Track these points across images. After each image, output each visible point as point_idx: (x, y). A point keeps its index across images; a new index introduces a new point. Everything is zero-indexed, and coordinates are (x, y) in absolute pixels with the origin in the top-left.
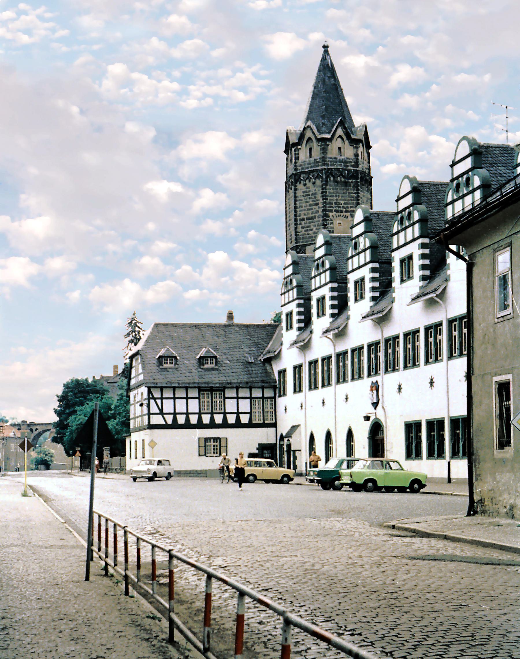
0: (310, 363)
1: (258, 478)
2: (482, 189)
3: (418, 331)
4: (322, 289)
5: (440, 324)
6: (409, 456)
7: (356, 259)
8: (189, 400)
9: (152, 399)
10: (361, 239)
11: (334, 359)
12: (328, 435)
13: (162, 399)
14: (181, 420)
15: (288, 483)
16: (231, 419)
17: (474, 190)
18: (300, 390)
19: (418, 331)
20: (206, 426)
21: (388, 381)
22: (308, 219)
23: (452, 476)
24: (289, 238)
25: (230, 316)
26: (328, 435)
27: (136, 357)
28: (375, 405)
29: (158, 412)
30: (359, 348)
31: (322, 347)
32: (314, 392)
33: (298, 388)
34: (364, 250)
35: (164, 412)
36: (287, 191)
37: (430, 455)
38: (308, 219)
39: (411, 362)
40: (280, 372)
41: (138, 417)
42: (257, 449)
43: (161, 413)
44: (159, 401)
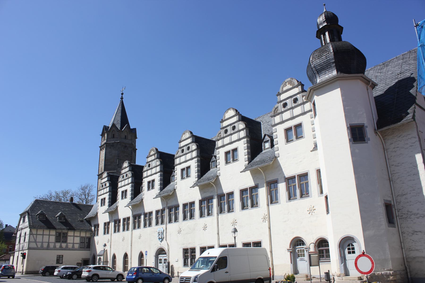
1: (100, 277)
4: (125, 184)
10: (153, 162)
12: (126, 256)
13: (37, 234)
14: (45, 245)
15: (121, 281)
16: (70, 246)
17: (192, 151)
20: (70, 250)
21: (172, 227)
25: (72, 199)
26: (126, 256)
28: (162, 239)
34: (156, 166)
35: (37, 241)
39: (126, 228)
41: (36, 244)
43: (36, 242)
44: (35, 236)
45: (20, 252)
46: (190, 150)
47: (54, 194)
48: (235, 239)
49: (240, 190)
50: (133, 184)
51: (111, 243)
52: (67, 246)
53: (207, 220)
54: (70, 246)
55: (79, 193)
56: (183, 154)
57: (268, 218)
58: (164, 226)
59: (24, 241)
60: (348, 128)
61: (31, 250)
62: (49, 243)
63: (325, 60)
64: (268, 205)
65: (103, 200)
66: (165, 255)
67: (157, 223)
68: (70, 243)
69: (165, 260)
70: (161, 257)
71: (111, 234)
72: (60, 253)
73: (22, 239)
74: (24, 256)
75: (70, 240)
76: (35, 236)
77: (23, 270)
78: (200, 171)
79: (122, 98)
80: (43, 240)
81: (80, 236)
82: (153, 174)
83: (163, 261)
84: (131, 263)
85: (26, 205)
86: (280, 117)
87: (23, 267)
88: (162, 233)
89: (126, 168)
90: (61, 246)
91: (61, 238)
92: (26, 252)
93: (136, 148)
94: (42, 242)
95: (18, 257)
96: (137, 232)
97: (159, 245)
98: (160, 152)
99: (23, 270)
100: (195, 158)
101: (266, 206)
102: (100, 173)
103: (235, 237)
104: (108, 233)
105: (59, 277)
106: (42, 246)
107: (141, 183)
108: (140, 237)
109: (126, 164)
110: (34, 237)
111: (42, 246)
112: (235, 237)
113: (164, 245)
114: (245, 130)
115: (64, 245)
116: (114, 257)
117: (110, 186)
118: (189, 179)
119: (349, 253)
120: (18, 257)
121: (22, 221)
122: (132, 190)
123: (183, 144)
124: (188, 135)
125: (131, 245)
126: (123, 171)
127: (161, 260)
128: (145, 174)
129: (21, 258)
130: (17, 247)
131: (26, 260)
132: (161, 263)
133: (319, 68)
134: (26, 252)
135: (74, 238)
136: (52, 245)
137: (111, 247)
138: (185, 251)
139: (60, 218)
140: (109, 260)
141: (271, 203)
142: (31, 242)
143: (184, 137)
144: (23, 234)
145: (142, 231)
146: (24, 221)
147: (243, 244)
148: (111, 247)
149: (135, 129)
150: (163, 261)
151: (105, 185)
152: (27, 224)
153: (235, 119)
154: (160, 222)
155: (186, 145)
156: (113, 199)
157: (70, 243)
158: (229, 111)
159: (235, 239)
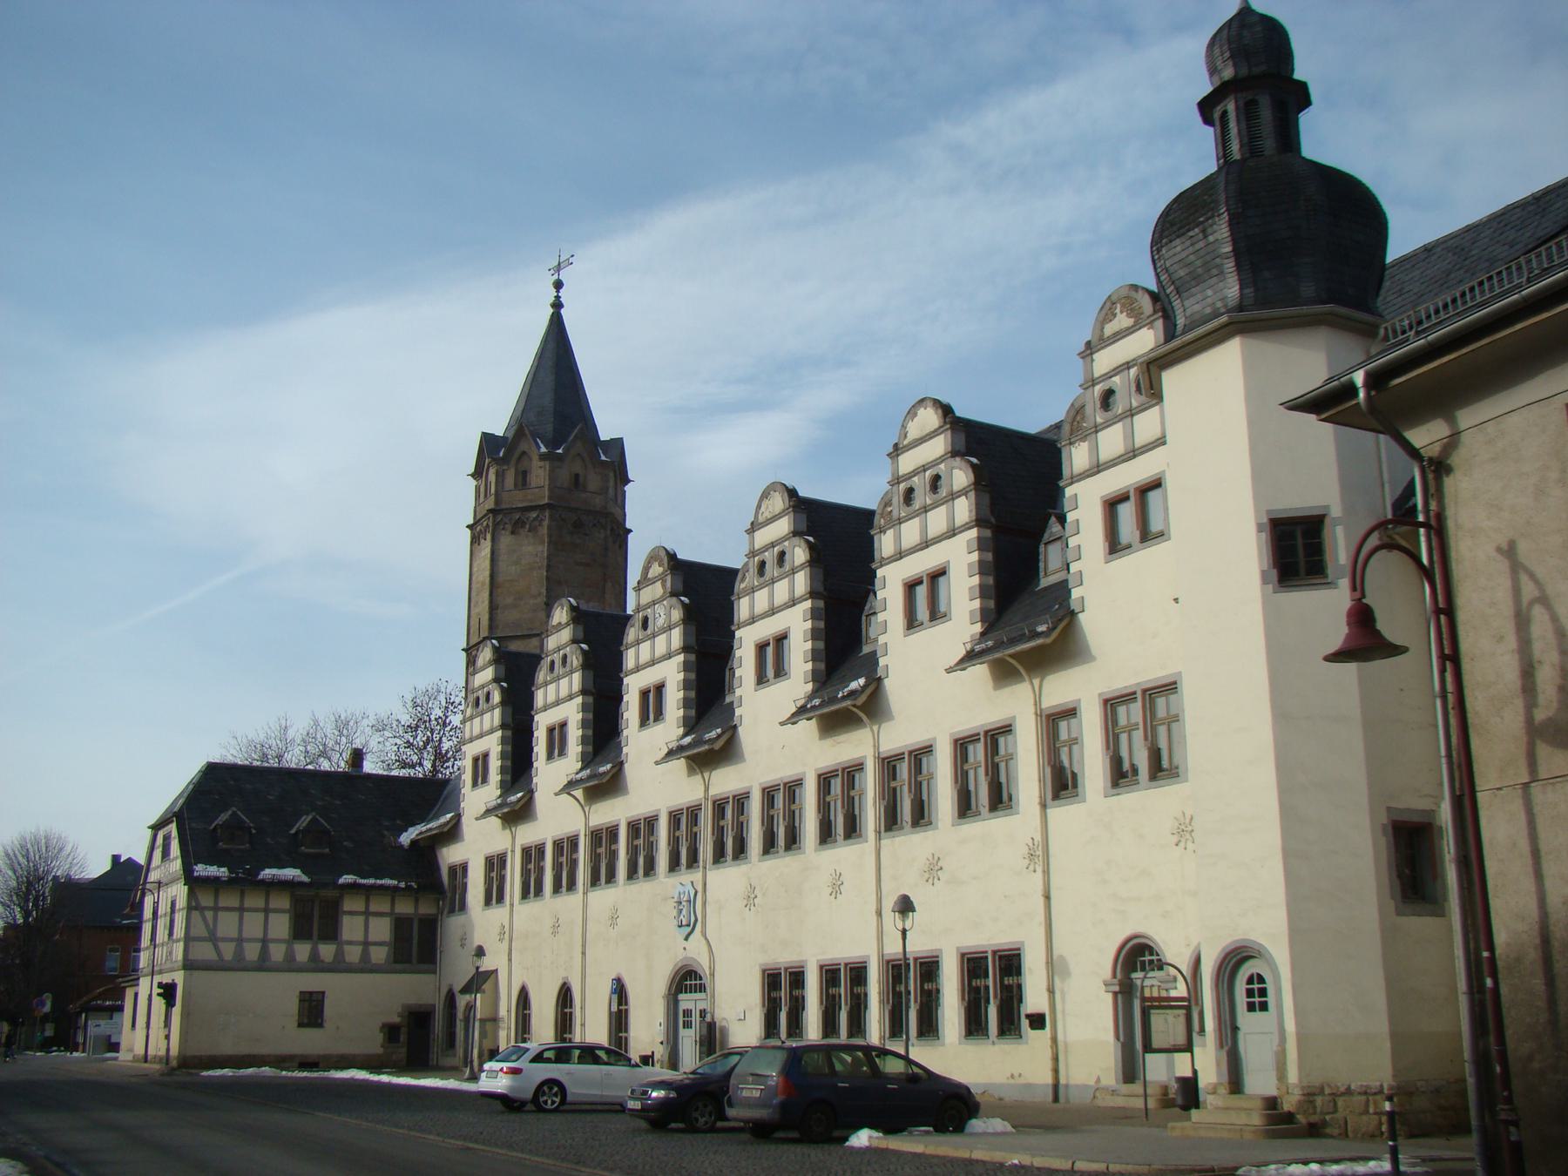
0: (526, 852)
3: (928, 750)
4: (560, 702)
5: (859, 767)
8: (272, 916)
9: (196, 908)
11: (755, 807)
12: (565, 996)
13: (216, 909)
14: (252, 952)
16: (353, 954)
17: (953, 496)
19: (928, 750)
20: (301, 969)
24: (474, 622)
26: (565, 996)
29: (206, 934)
30: (1144, 691)
31: (558, 813)
33: (495, 894)
34: (670, 628)
35: (220, 934)
36: (475, 540)
39: (565, 882)
40: (453, 870)
42: (399, 1015)
43: (213, 938)
45: (157, 979)
46: (943, 492)
47: (298, 729)
48: (904, 938)
49: (956, 741)
50: (509, 733)
51: (511, 941)
52: (339, 954)
53: (844, 855)
54: (353, 954)
55: (406, 719)
56: (1109, 414)
57: (1041, 854)
58: (697, 876)
59: (171, 934)
60: (1260, 528)
61: (196, 973)
62: (265, 941)
63: (1201, 244)
64: (1044, 806)
65: (481, 762)
66: (702, 995)
67: (674, 865)
68: (350, 943)
69: (703, 1013)
70: (687, 1001)
71: (512, 905)
73: (162, 924)
74: (168, 992)
75: (351, 928)
76: (209, 915)
77: (168, 1050)
78: (993, 592)
79: (557, 305)
80: (240, 931)
81: (391, 914)
82: (656, 661)
83: (696, 1019)
84: (583, 1025)
85: (172, 781)
86: (1090, 450)
87: (167, 1037)
88: (691, 902)
89: (559, 627)
90: (314, 956)
91: (316, 918)
92: (178, 977)
93: (628, 526)
94: (240, 940)
95: (150, 996)
96: (603, 898)
97: (681, 955)
98: (960, 420)
99: (168, 1050)
100: (966, 527)
101: (1038, 808)
102: (473, 642)
103: (904, 932)
104: (500, 899)
106: (239, 952)
107: (618, 698)
108: (614, 919)
109: (560, 615)
110: (204, 919)
111: (239, 952)
112: (904, 932)
113: (696, 950)
114: (972, 495)
115: (327, 951)
116: (524, 999)
117: (503, 703)
119: (1251, 1007)
120: (150, 996)
121: (158, 854)
122: (686, 685)
123: (907, 462)
124: (929, 418)
125: (584, 953)
126: (552, 642)
127: (687, 1013)
128: (743, 608)
129: (159, 1004)
130: (144, 959)
131: (177, 1011)
132: (687, 1025)
133: (1182, 273)
134: (178, 977)
135: (366, 927)
136: (277, 953)
137: (510, 960)
138: (772, 980)
139: (309, 837)
140: (503, 1012)
141: (1056, 797)
143: (914, 430)
144: (164, 908)
145: (622, 896)
146: (166, 853)
147: (963, 955)
148: (510, 960)
149: (617, 445)
150: (696, 1019)
151: (488, 699)
153: (939, 446)
154: (684, 860)
155: (773, 545)
156: (519, 766)
157: (350, 943)
158: (921, 412)
159: (904, 938)
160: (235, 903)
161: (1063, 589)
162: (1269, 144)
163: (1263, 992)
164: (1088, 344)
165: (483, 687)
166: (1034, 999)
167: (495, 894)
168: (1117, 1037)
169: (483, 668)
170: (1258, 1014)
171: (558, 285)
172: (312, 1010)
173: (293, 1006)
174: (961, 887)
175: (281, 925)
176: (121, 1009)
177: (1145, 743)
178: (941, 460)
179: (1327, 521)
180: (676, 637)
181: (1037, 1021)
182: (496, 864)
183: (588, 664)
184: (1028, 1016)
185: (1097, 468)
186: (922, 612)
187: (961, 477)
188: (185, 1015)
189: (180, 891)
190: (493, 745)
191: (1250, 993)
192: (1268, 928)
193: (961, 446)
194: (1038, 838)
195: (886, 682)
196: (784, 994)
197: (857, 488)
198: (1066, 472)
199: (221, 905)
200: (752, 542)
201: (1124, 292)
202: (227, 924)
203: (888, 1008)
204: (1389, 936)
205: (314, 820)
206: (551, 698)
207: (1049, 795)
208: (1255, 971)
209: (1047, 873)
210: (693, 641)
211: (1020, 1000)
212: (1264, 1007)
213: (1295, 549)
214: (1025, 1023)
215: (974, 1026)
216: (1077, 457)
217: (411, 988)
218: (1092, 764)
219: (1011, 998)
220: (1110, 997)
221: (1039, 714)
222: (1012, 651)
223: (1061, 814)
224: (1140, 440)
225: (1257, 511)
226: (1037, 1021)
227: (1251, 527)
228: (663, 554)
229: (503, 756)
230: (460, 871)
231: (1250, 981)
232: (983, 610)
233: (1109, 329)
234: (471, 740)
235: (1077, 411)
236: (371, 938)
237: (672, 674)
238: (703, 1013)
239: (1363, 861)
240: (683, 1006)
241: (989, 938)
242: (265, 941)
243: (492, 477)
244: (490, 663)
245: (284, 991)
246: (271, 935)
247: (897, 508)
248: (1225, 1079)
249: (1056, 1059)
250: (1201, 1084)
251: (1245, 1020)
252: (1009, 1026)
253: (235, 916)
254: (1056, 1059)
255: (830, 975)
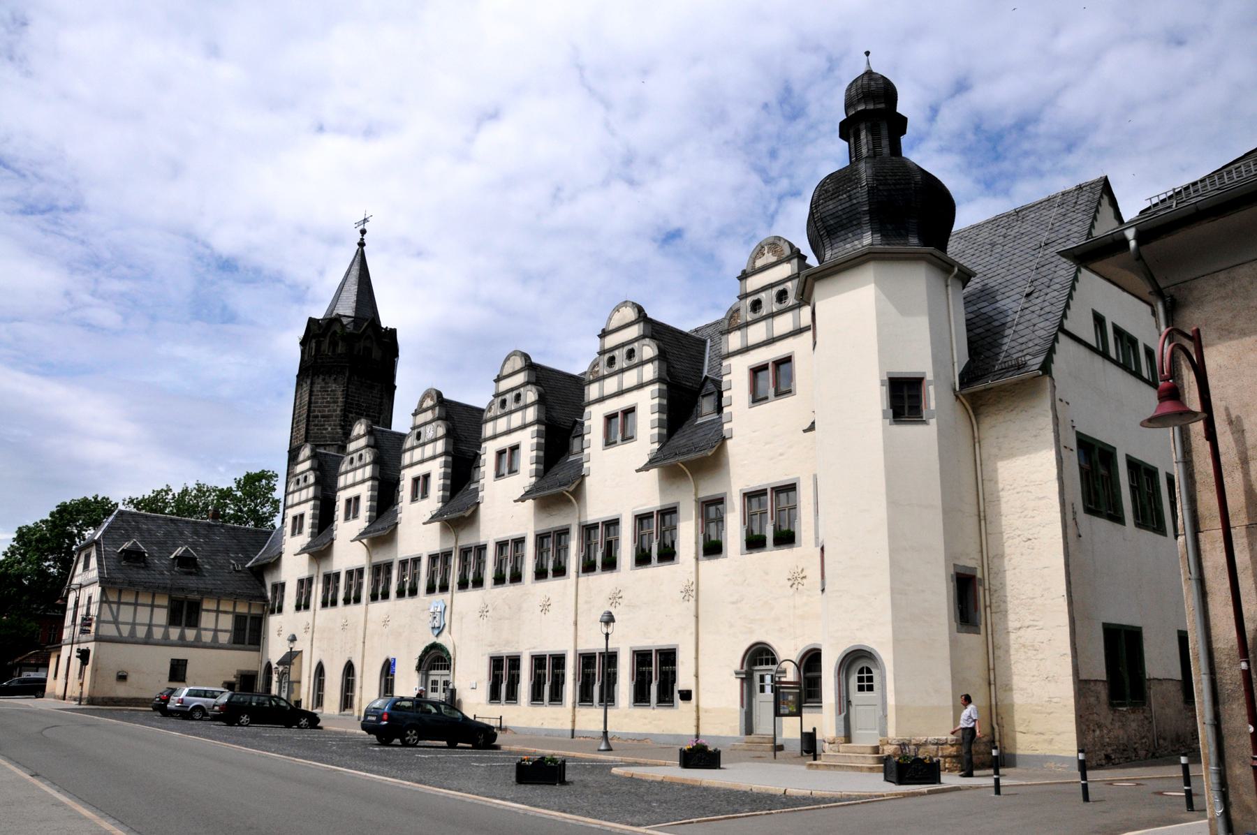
2: (656, 363)
4: (356, 483)
6: (494, 696)
7: (297, 494)
12: (349, 669)
13: (119, 603)
14: (141, 632)
16: (207, 637)
17: (526, 407)
18: (307, 607)
20: (205, 646)
22: (323, 417)
23: (577, 728)
26: (349, 669)
27: (87, 551)
32: (330, 611)
33: (303, 604)
34: (435, 440)
35: (121, 619)
36: (299, 385)
37: (537, 696)
38: (323, 417)
39: (353, 598)
43: (116, 622)
45: (75, 647)
50: (376, 483)
52: (198, 637)
54: (207, 637)
57: (693, 592)
58: (446, 596)
62: (150, 626)
64: (697, 559)
65: (298, 520)
72: (180, 653)
74: (84, 655)
75: (207, 620)
76: (114, 607)
79: (362, 244)
82: (426, 461)
87: (82, 684)
88: (443, 613)
90: (182, 637)
91: (184, 613)
103: (607, 635)
104: (307, 607)
105: (74, 704)
106: (133, 632)
107: (397, 482)
108: (386, 623)
110: (111, 609)
111: (133, 632)
112: (607, 635)
115: (190, 634)
116: (320, 670)
118: (425, 502)
119: (861, 689)
126: (352, 446)
127: (435, 683)
128: (407, 458)
129: (76, 663)
131: (88, 668)
134: (91, 646)
135: (217, 621)
136: (158, 633)
138: (496, 662)
142: (104, 622)
144: (83, 601)
152: (93, 574)
155: (512, 390)
160: (132, 600)
161: (476, 491)
162: (886, 150)
163: (870, 679)
164: (744, 272)
165: (357, 451)
166: (684, 680)
167: (303, 604)
168: (742, 706)
169: (304, 461)
170: (866, 694)
171: (363, 232)
172: (178, 671)
173: (167, 668)
174: (639, 607)
175: (161, 616)
176: (47, 666)
177: (775, 521)
178: (636, 340)
179: (925, 383)
180: (440, 446)
181: (686, 696)
182: (305, 585)
183: (376, 462)
184: (680, 692)
185: (602, 399)
186: (505, 469)
187: (531, 395)
188: (95, 671)
189: (95, 591)
190: (308, 510)
191: (860, 679)
192: (878, 638)
193: (648, 332)
194: (693, 579)
195: (587, 480)
196: (505, 672)
197: (477, 396)
198: (586, 399)
199: (123, 600)
200: (497, 388)
201: (771, 241)
202: (126, 614)
203: (579, 684)
204: (953, 644)
205: (187, 551)
206: (350, 481)
207: (701, 552)
208: (865, 665)
209: (697, 601)
210: (451, 449)
211: (674, 681)
212: (870, 688)
213: (904, 398)
214: (677, 696)
215: (641, 696)
216: (593, 391)
217: (243, 660)
218: (733, 531)
219: (668, 680)
220: (738, 681)
221: (697, 501)
222: (682, 458)
223: (709, 565)
224: (777, 333)
225: (881, 371)
226: (686, 696)
227: (878, 383)
228: (434, 393)
229: (314, 517)
230: (280, 588)
231: (861, 671)
232: (443, 497)
233: (759, 263)
234: (292, 506)
235: (734, 313)
236: (220, 627)
237: (365, 492)
238: (446, 683)
239: (939, 597)
240: (431, 678)
241: (654, 641)
242: (150, 626)
243: (313, 345)
244: (309, 458)
245: (162, 658)
246: (154, 622)
247: (496, 410)
248: (842, 734)
249: (698, 719)
250: (818, 737)
251: (856, 696)
252: (666, 697)
253: (131, 608)
254: (698, 719)
255: (539, 661)
